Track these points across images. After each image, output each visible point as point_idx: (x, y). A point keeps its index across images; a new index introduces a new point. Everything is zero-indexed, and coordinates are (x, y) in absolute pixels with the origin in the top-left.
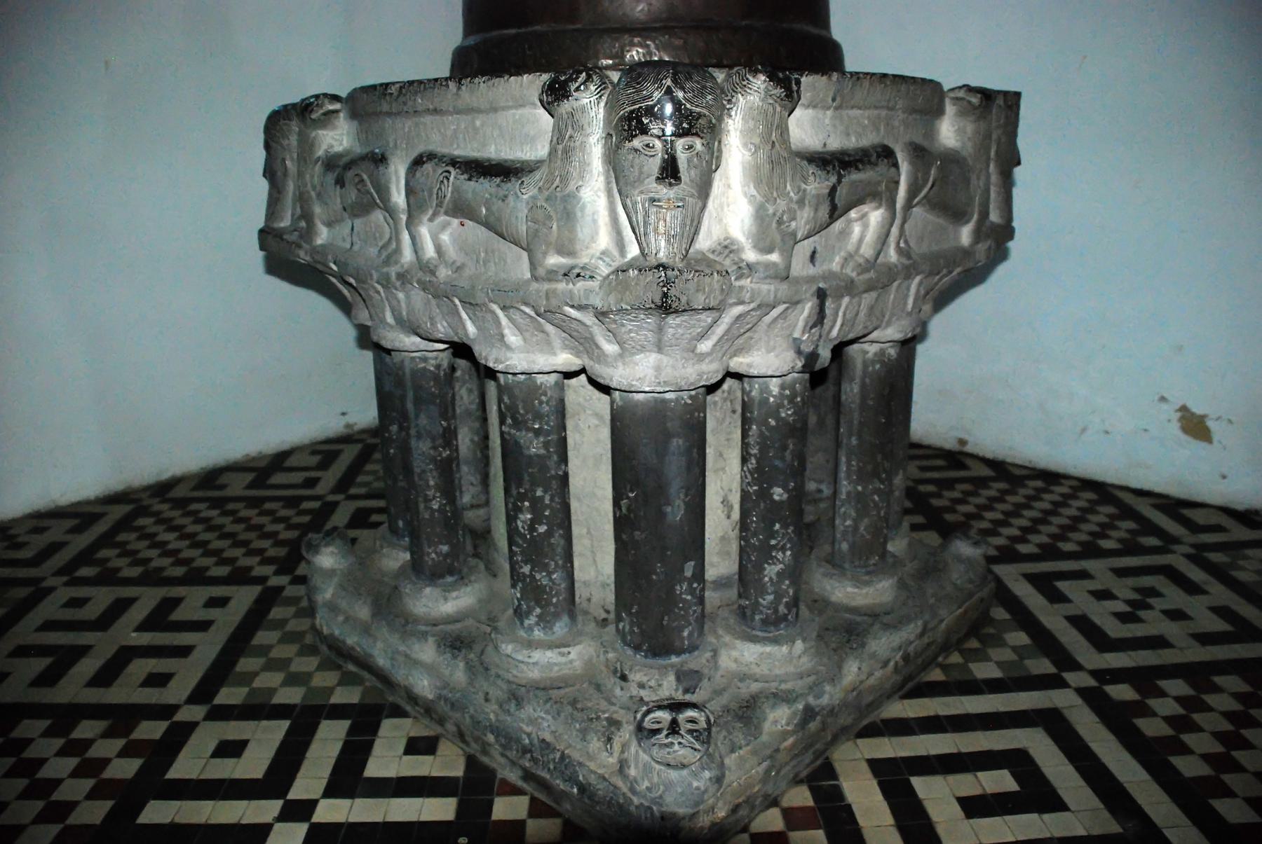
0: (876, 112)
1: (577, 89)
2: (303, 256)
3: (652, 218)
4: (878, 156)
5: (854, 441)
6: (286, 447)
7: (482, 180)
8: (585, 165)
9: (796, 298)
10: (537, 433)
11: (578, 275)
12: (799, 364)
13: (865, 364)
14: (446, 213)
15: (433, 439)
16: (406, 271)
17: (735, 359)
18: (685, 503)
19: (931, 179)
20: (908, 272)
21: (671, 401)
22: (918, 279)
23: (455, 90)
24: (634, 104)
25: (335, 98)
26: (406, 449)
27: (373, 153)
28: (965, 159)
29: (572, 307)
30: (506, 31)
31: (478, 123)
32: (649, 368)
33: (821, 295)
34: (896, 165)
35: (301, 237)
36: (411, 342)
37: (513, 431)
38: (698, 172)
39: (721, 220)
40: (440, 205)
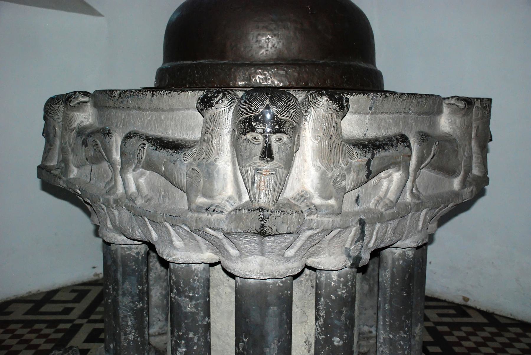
0: (397, 115)
1: (217, 102)
2: (62, 184)
3: (256, 178)
4: (398, 141)
5: (387, 306)
6: (56, 287)
7: (162, 150)
8: (220, 145)
9: (346, 225)
10: (191, 299)
11: (214, 210)
12: (349, 263)
13: (394, 261)
14: (143, 167)
15: (133, 297)
16: (119, 199)
17: (310, 259)
18: (279, 347)
19: (432, 153)
20: (418, 208)
21: (269, 284)
22: (424, 211)
23: (150, 97)
24: (247, 114)
25: (86, 94)
26: (116, 302)
27: (104, 129)
28: (455, 139)
29: (210, 228)
30: (185, 62)
31: (163, 117)
32: (258, 265)
33: (362, 223)
34: (409, 146)
35: (62, 173)
36: (121, 239)
37: (177, 297)
38: (284, 154)
39: (299, 180)
40: (139, 162)
